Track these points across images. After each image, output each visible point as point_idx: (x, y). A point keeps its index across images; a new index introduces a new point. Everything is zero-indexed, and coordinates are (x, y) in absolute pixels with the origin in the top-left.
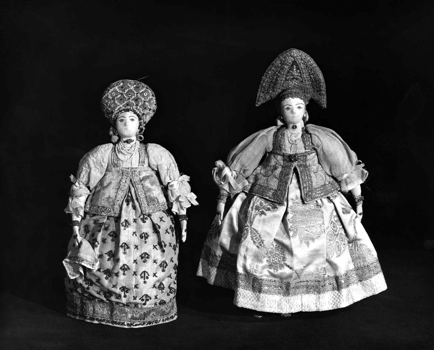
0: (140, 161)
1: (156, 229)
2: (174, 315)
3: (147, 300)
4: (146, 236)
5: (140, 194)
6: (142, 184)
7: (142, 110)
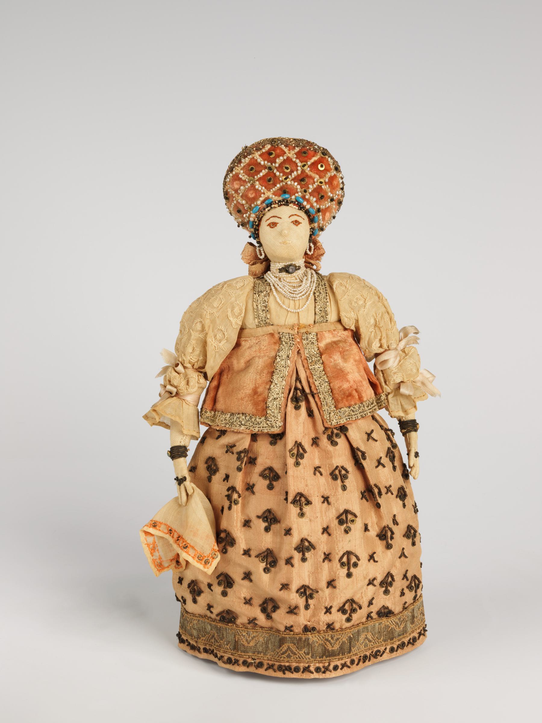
0: (317, 310)
1: (357, 456)
2: (417, 636)
3: (354, 611)
4: (343, 472)
5: (317, 383)
6: (323, 363)
7: (316, 201)
